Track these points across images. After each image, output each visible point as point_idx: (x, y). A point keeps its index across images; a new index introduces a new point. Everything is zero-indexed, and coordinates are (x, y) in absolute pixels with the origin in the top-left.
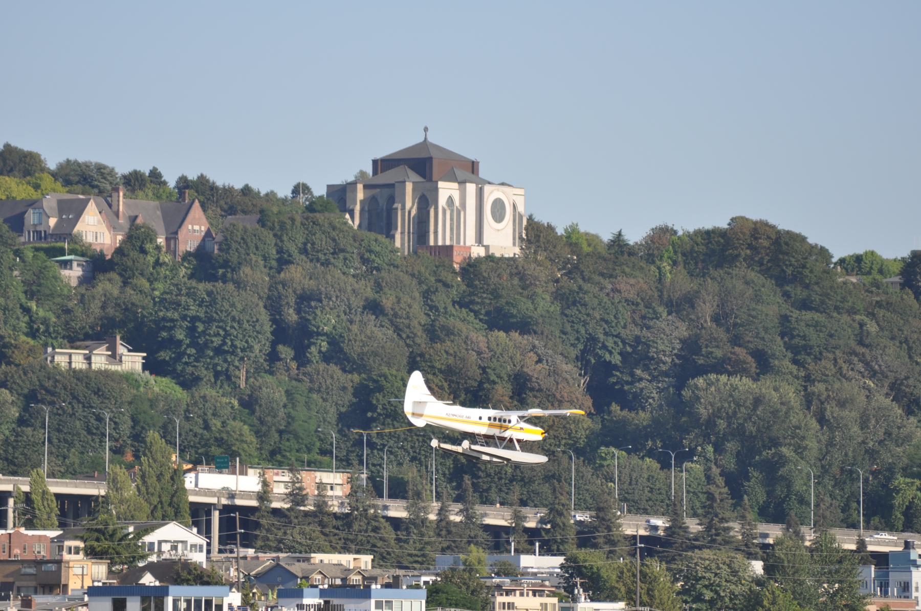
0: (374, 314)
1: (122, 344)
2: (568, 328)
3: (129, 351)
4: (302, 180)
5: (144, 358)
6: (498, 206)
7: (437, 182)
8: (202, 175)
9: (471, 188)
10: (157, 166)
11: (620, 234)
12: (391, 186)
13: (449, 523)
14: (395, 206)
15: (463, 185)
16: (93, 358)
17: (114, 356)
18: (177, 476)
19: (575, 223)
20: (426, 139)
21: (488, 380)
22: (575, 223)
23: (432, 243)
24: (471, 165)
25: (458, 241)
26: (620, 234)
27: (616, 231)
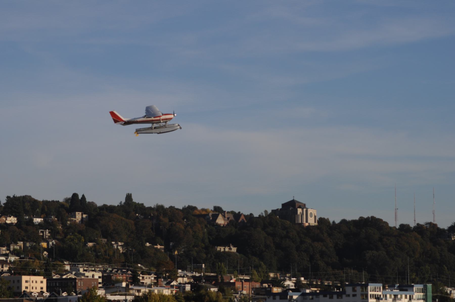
2: (331, 240)
3: (233, 247)
6: (311, 214)
8: (131, 194)
9: (305, 210)
10: (215, 205)
11: (129, 197)
17: (230, 249)
19: (130, 193)
22: (130, 193)
23: (296, 222)
27: (83, 194)
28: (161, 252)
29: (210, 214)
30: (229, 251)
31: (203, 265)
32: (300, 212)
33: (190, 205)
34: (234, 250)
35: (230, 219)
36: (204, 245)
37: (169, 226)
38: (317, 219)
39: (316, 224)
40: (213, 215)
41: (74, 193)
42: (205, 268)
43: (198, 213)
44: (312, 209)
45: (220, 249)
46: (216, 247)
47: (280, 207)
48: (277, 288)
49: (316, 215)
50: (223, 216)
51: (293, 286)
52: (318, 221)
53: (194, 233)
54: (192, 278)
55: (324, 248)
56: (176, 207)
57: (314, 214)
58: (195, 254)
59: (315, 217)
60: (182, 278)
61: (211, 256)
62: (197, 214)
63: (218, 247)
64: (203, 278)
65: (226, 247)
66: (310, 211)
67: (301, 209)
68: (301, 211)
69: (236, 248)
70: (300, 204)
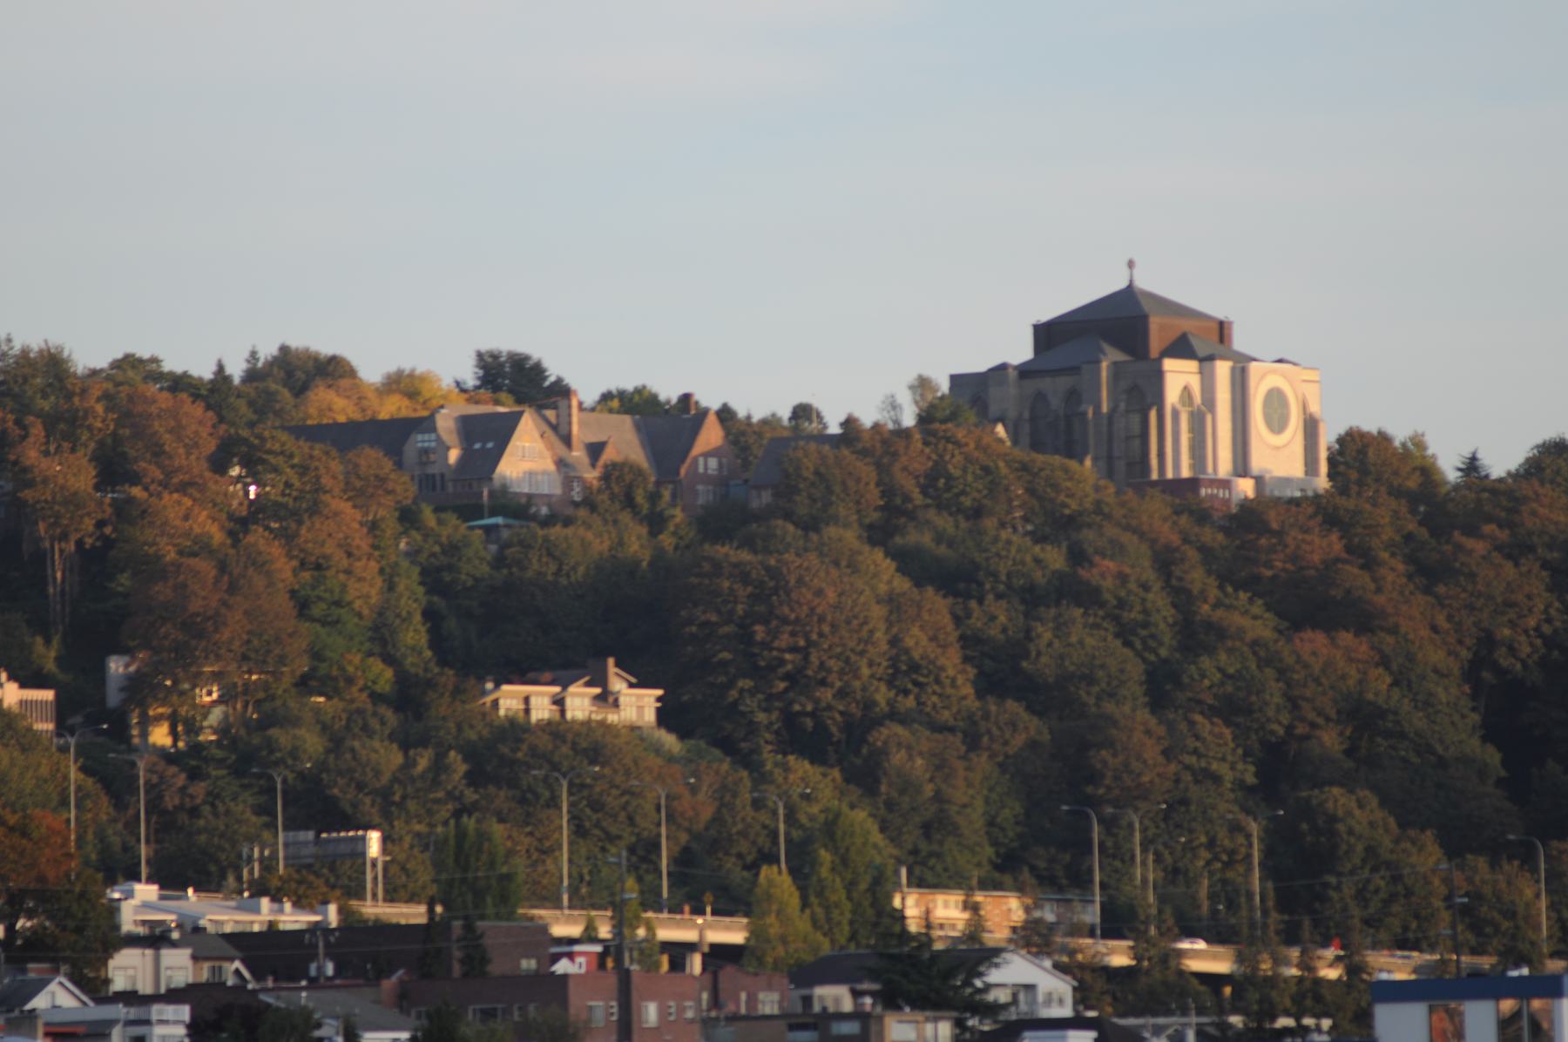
0: (1079, 605)
1: (617, 674)
2: (1441, 619)
3: (631, 686)
4: (805, 399)
5: (659, 699)
6: (1276, 399)
7: (1159, 360)
9: (1223, 369)
10: (487, 345)
11: (1473, 459)
12: (1074, 370)
13: (1319, 982)
14: (1082, 408)
15: (1207, 364)
16: (569, 702)
17: (606, 699)
18: (880, 887)
20: (1131, 281)
21: (1303, 719)
23: (1155, 476)
24: (1216, 326)
25: (1203, 469)
26: (1473, 459)
28: (27, 742)
29: (446, 423)
30: (597, 717)
31: (374, 839)
32: (1186, 390)
33: (296, 342)
34: (640, 708)
35: (609, 455)
36: (389, 673)
37: (100, 524)
38: (1328, 437)
39: (1322, 482)
40: (469, 428)
41: (407, 366)
42: (386, 866)
43: (341, 408)
44: (1280, 361)
45: (527, 700)
46: (489, 686)
47: (1021, 351)
48: (919, 1016)
49: (1314, 408)
50: (549, 433)
51: (1061, 1002)
52: (1332, 461)
53: (306, 576)
54: (233, 952)
55: (1379, 684)
56: (172, 364)
57: (1305, 407)
58: (312, 743)
59: (1311, 427)
60: (149, 952)
61: (439, 767)
62: (342, 419)
63: (505, 688)
64: (321, 950)
65: (572, 689)
66: (1263, 381)
67: (1192, 365)
68: (1195, 383)
69: (660, 692)
70: (1186, 325)
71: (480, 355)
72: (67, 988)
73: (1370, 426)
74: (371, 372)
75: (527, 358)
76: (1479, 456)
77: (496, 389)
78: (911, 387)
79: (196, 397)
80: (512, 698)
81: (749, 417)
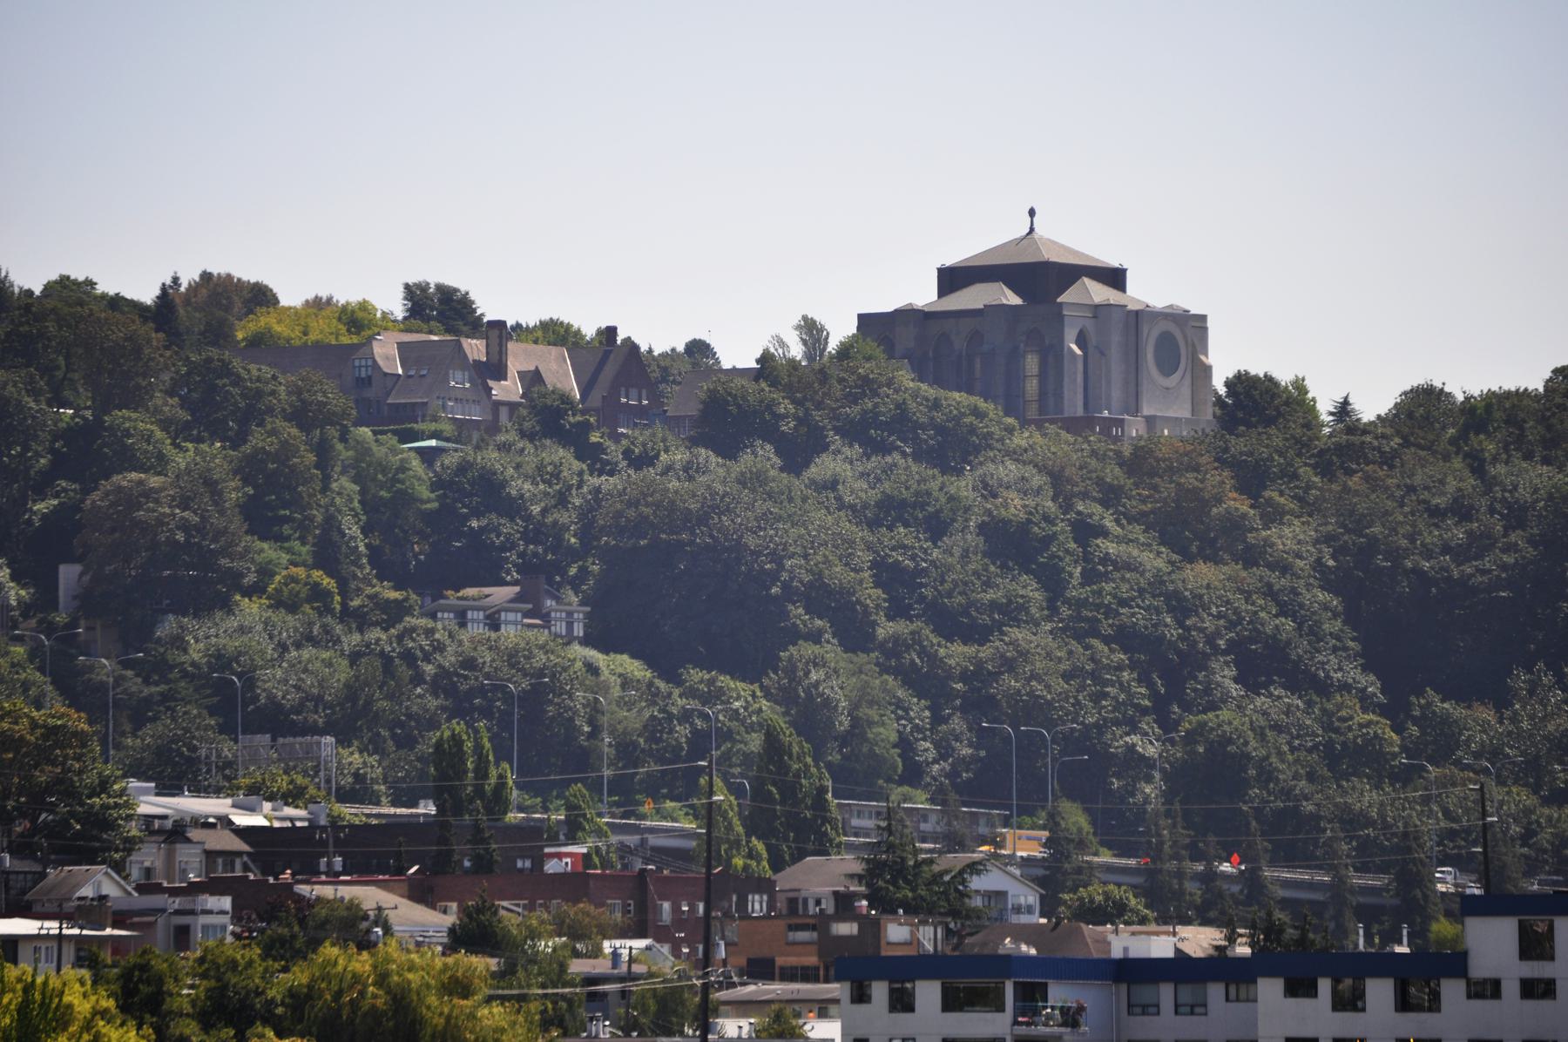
11: (1346, 402)
26: (1346, 402)
33: (217, 269)
71: (407, 287)
72: (112, 878)
73: (1257, 370)
74: (291, 296)
75: (456, 290)
76: (1351, 400)
77: (427, 319)
78: (798, 327)
79: (1518, 444)
80: (449, 612)
81: (650, 351)
